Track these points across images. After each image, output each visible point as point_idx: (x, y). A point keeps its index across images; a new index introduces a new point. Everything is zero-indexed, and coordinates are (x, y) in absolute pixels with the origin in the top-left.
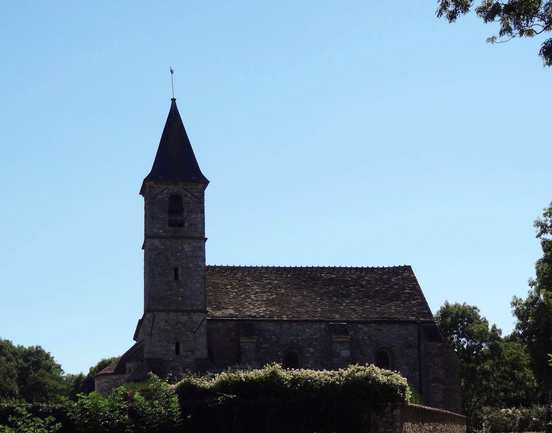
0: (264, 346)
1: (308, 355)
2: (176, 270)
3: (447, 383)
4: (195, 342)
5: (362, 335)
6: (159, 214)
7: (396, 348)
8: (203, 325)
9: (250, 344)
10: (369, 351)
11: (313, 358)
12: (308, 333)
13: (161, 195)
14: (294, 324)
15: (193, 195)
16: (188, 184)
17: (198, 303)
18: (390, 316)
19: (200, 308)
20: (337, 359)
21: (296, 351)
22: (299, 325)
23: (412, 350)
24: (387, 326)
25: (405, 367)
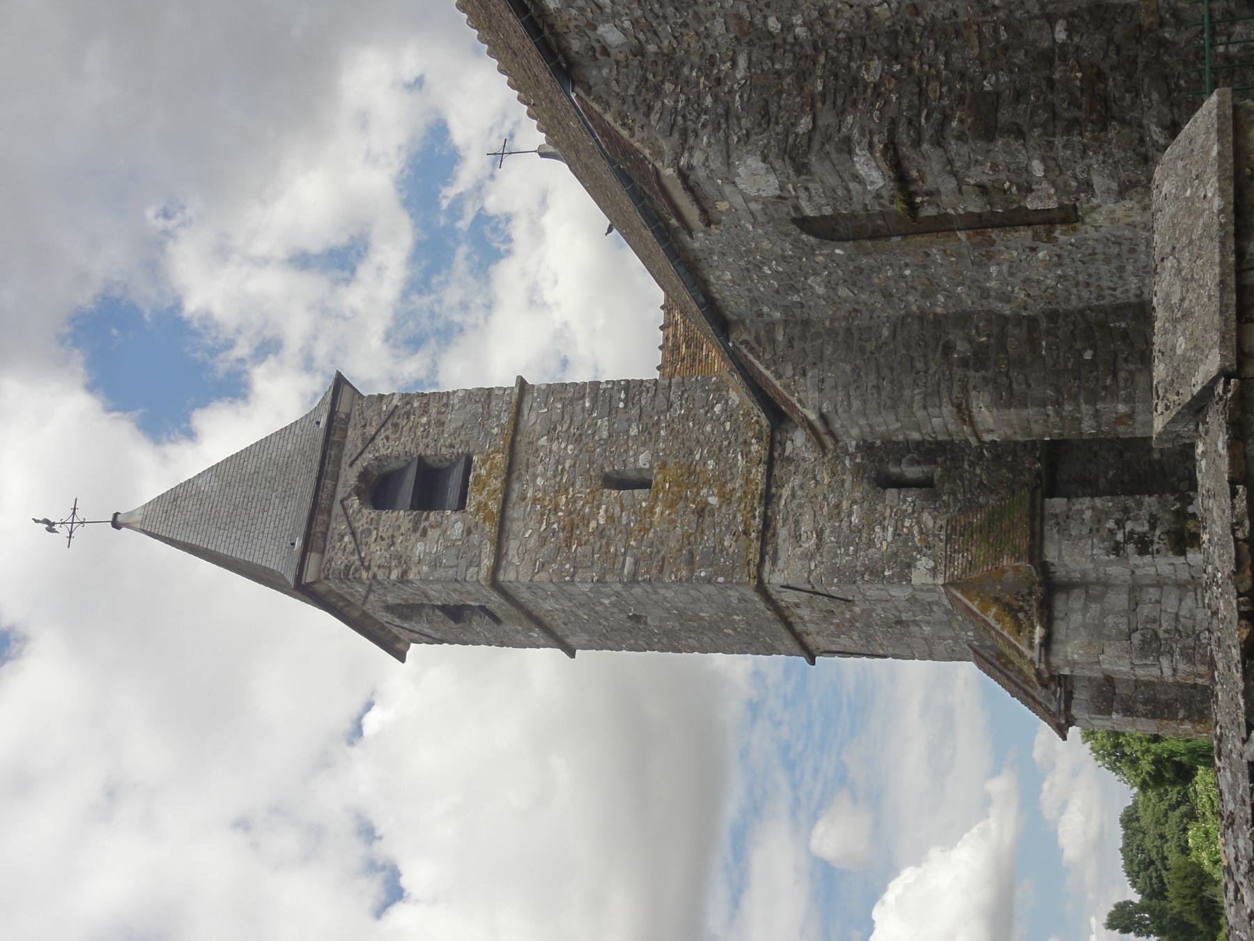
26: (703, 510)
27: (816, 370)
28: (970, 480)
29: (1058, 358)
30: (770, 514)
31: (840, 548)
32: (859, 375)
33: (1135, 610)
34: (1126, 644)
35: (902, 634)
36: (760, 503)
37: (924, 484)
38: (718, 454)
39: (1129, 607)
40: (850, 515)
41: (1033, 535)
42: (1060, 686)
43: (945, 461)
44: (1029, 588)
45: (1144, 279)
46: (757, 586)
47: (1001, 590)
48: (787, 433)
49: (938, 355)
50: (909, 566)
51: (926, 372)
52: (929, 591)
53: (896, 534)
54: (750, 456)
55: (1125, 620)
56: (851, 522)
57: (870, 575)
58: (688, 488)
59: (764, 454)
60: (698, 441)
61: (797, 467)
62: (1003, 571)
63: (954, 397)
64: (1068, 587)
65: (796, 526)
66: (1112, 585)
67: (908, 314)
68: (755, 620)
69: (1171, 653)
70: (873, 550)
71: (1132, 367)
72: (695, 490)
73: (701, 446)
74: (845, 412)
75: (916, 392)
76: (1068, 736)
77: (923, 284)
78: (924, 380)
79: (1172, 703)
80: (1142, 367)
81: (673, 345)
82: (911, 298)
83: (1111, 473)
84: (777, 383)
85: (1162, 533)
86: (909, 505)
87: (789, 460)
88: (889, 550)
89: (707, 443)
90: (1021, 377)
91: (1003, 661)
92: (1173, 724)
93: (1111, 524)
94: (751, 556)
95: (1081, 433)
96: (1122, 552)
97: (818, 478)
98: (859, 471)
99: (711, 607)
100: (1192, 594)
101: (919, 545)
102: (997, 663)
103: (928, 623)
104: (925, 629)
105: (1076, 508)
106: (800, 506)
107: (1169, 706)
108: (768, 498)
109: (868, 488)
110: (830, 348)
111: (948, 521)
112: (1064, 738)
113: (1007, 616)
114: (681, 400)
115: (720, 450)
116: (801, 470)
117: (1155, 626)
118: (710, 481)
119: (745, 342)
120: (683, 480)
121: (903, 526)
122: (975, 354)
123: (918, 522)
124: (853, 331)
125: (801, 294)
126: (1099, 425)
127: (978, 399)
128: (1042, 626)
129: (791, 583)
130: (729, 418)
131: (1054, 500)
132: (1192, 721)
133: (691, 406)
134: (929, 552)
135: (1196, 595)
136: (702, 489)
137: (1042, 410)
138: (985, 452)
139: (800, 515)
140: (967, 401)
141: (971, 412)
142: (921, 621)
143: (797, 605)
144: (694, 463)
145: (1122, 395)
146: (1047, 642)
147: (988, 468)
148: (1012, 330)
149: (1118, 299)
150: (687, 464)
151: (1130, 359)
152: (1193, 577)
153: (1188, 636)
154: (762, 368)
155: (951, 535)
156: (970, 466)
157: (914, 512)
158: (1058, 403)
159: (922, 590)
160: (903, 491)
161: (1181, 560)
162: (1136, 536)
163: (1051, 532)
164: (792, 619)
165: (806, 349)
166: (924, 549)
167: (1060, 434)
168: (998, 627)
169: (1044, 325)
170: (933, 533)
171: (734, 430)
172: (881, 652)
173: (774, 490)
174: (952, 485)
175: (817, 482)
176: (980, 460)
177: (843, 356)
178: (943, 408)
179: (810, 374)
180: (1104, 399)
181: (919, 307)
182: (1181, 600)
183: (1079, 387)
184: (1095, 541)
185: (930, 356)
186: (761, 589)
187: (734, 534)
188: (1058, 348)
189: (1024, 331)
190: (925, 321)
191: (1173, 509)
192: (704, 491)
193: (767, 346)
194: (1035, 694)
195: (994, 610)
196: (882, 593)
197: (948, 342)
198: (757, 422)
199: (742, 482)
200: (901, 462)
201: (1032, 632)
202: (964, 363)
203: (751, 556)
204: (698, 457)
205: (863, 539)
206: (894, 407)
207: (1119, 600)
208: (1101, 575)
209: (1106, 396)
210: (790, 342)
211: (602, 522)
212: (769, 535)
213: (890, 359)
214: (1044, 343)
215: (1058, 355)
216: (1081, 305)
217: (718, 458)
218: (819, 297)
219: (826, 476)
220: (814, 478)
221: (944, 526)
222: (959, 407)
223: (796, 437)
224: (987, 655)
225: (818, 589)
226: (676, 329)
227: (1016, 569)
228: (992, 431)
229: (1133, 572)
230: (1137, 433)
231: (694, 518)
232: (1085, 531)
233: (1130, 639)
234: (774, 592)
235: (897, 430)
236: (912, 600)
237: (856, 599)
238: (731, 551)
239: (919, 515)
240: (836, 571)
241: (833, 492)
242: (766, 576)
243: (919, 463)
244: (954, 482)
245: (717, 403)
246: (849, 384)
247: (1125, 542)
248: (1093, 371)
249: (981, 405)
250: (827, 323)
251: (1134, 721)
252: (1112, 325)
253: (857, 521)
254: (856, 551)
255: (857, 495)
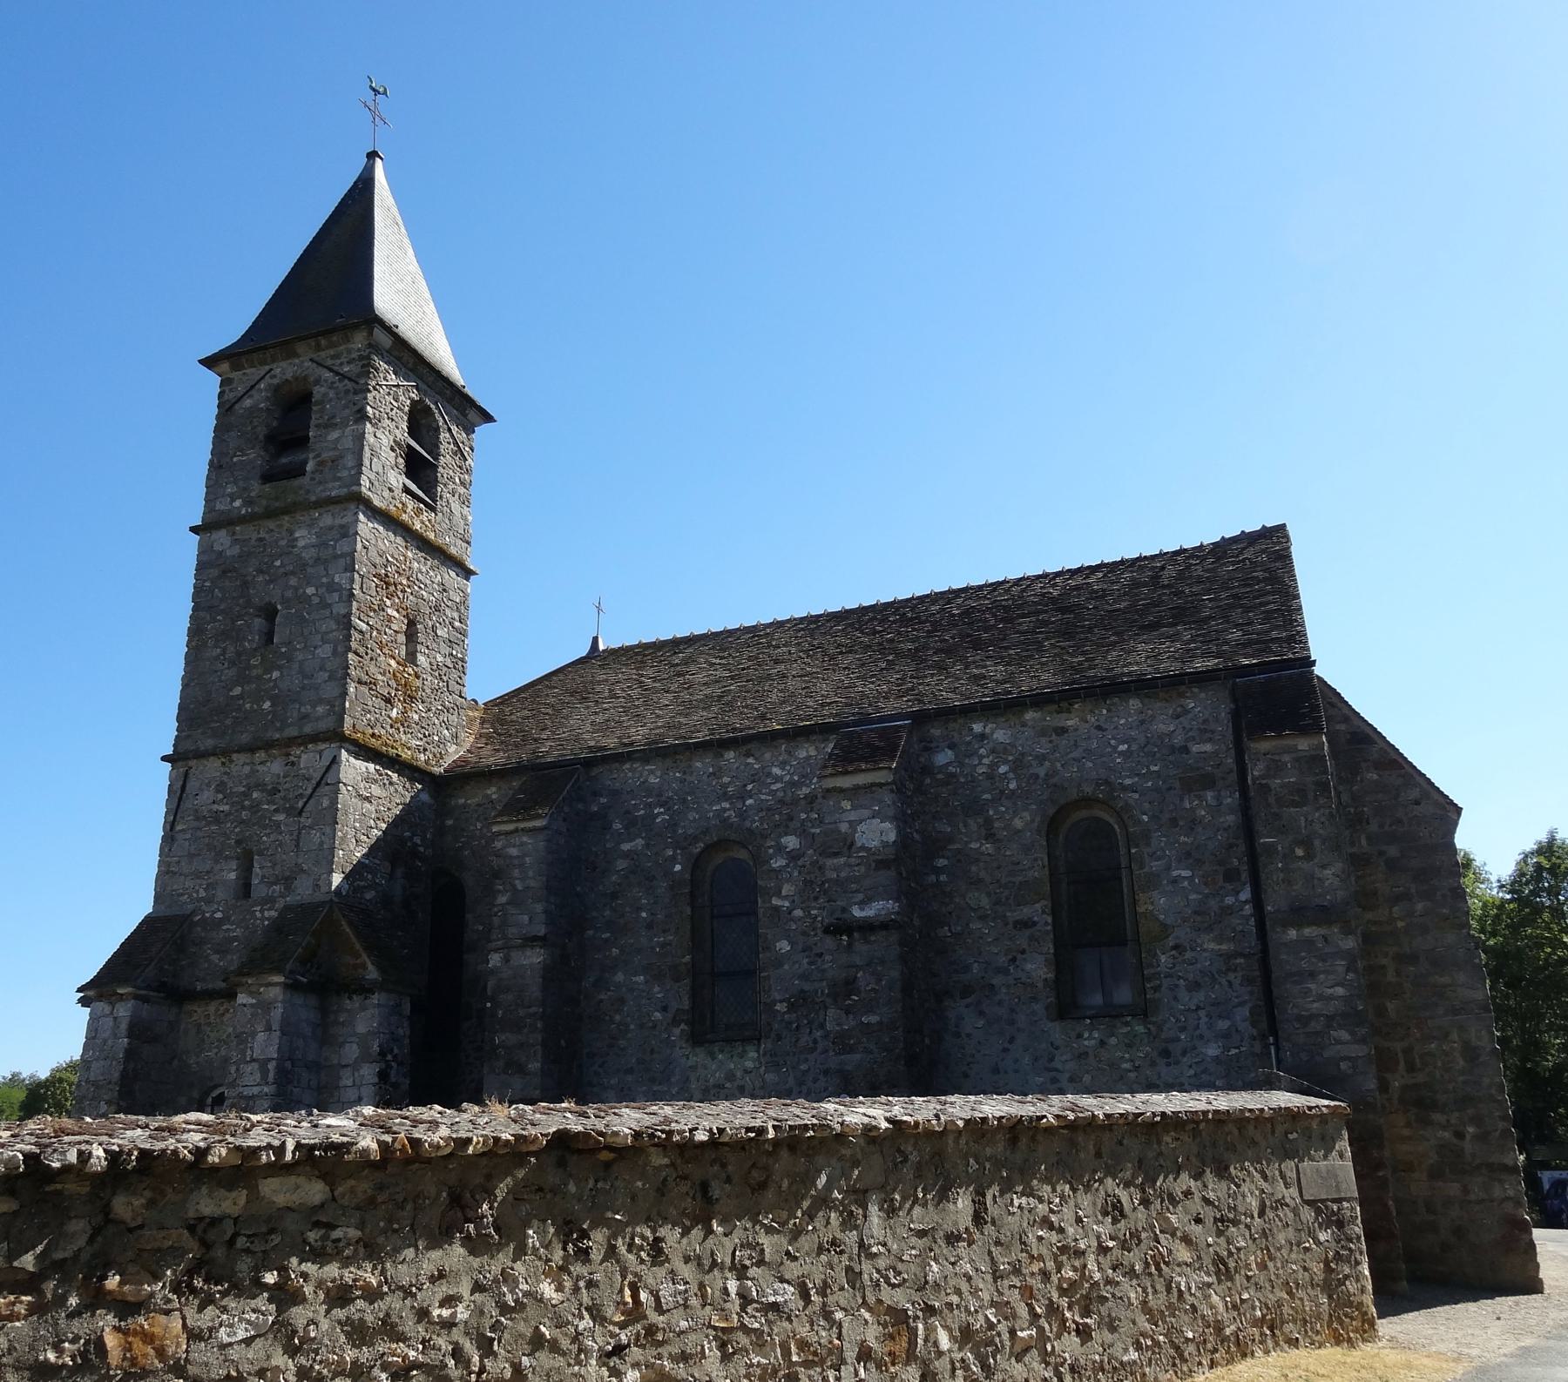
0: (626, 847)
1: (778, 865)
2: (270, 613)
3: (1400, 924)
4: (297, 846)
5: (986, 761)
6: (238, 453)
7: (1136, 796)
8: (328, 784)
9: (525, 839)
10: (1018, 823)
11: (796, 874)
12: (778, 779)
13: (251, 396)
14: (730, 755)
15: (337, 373)
16: (323, 342)
17: (320, 709)
18: (1108, 672)
19: (323, 726)
20: (842, 860)
21: (742, 854)
22: (748, 755)
23: (1209, 795)
24: (1092, 712)
25: (1185, 873)
55: (300, 1057)
102: (177, 935)
211: (390, 611)
228: (507, 961)
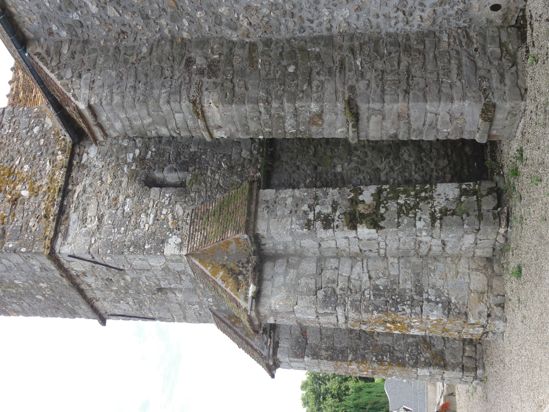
26: (16, 200)
27: (90, 74)
28: (211, 183)
29: (270, 71)
30: (65, 203)
31: (114, 228)
32: (121, 78)
33: (320, 274)
34: (313, 298)
35: (163, 300)
36: (58, 195)
37: (182, 185)
38: (32, 161)
39: (316, 272)
40: (124, 205)
41: (249, 214)
42: (271, 338)
43: (195, 170)
44: (247, 258)
45: (333, 12)
46: (49, 254)
47: (227, 260)
48: (85, 148)
49: (182, 66)
50: (163, 242)
51: (171, 78)
52: (177, 261)
53: (156, 219)
54: (56, 163)
55: (313, 281)
56: (124, 210)
57: (134, 248)
58: (7, 184)
59: (66, 161)
60: (19, 152)
61: (89, 172)
62: (228, 243)
63: (191, 96)
64: (274, 257)
65: (83, 213)
66: (305, 257)
67: (162, 38)
68: (56, 288)
69: (344, 304)
70: (139, 230)
71: (322, 78)
72: (12, 186)
73: (21, 155)
74: (107, 104)
75: (163, 91)
76: (276, 375)
77: (171, 7)
78: (170, 83)
79: (344, 350)
80: (330, 78)
81: (15, 93)
82: (163, 22)
83: (308, 181)
84: (58, 83)
85: (341, 214)
86: (167, 199)
87: (84, 166)
88: (150, 230)
89: (25, 153)
90: (242, 83)
91: (233, 320)
92: (345, 365)
93: (305, 208)
94: (48, 233)
95: (285, 132)
96: (312, 227)
97: (104, 179)
98: (133, 176)
99: (21, 274)
100: (360, 263)
101: (171, 227)
102: (228, 322)
103: (181, 291)
104: (178, 295)
105: (281, 196)
106: (88, 198)
107: (342, 352)
108: (65, 192)
109: (138, 186)
110: (102, 59)
111: (193, 210)
112: (273, 376)
113: (230, 278)
114: (10, 123)
115: (34, 158)
116: (91, 173)
117: (334, 285)
118: (24, 179)
119: (38, 54)
120: (4, 179)
121: (161, 214)
122: (209, 66)
123: (172, 211)
124: (121, 48)
125: (79, 12)
126: (298, 125)
127: (209, 97)
128: (255, 284)
129: (77, 254)
130: (44, 136)
131: (266, 190)
132: (358, 362)
133: (17, 127)
134: (178, 232)
135: (363, 264)
136: (18, 185)
137: (256, 107)
138: (223, 164)
139: (88, 204)
140: (200, 98)
141: (202, 106)
142: (175, 289)
143: (84, 274)
144: (14, 167)
145: (314, 97)
146: (257, 296)
147: (224, 175)
148: (238, 51)
149: (314, 32)
150: (9, 167)
151: (321, 72)
152: (361, 250)
153: (356, 292)
154: (48, 72)
155: (194, 219)
156: (211, 174)
157: (169, 204)
158: (267, 102)
159: (172, 261)
160: (163, 190)
161: (352, 234)
162: (322, 216)
163: (262, 213)
164: (83, 286)
165: (84, 60)
166: (175, 230)
167: (271, 133)
168: (223, 286)
169: (261, 48)
170: (183, 219)
171: (46, 145)
172: (151, 316)
173: (70, 187)
174: (198, 186)
175: (102, 182)
176: (219, 169)
177: (111, 65)
178: (182, 103)
179: (84, 77)
180: (301, 99)
181: (170, 31)
182: (352, 268)
183: (283, 90)
184: (294, 219)
185: (176, 67)
186: (53, 256)
187: (37, 218)
188: (270, 64)
189: (246, 52)
190: (175, 43)
191: (349, 198)
192: (19, 187)
193: (54, 57)
194: (253, 344)
195: (221, 273)
196: (144, 263)
197: (190, 58)
198: (64, 139)
199: (48, 181)
200: (163, 169)
201: (247, 289)
202: (201, 72)
203: (48, 233)
204: (17, 163)
205: (132, 222)
206: (145, 102)
207: (309, 267)
208: (298, 248)
209: (303, 97)
210: (73, 54)
212: (63, 218)
213: (146, 68)
214: (260, 61)
215: (270, 68)
216: (288, 36)
217: (32, 164)
218: (93, 15)
219: (109, 178)
220: (101, 179)
221: (190, 214)
222: (194, 103)
223: (91, 150)
224: (222, 316)
225: (97, 259)
226: (18, 82)
227: (237, 240)
228: (220, 127)
229: (320, 245)
230: (325, 133)
231: (9, 205)
232: (287, 212)
233: (316, 295)
234: (65, 262)
235: (150, 125)
236: (166, 269)
237: (126, 268)
238: (34, 229)
239: (173, 206)
240: (110, 245)
241: (113, 189)
242: (57, 248)
243: (176, 170)
244: (200, 184)
245: (36, 126)
246: (113, 84)
247: (315, 220)
248: (294, 80)
249: (211, 101)
250: (102, 43)
251: (319, 362)
252: (309, 50)
253: (128, 209)
254: (126, 231)
255: (131, 192)
